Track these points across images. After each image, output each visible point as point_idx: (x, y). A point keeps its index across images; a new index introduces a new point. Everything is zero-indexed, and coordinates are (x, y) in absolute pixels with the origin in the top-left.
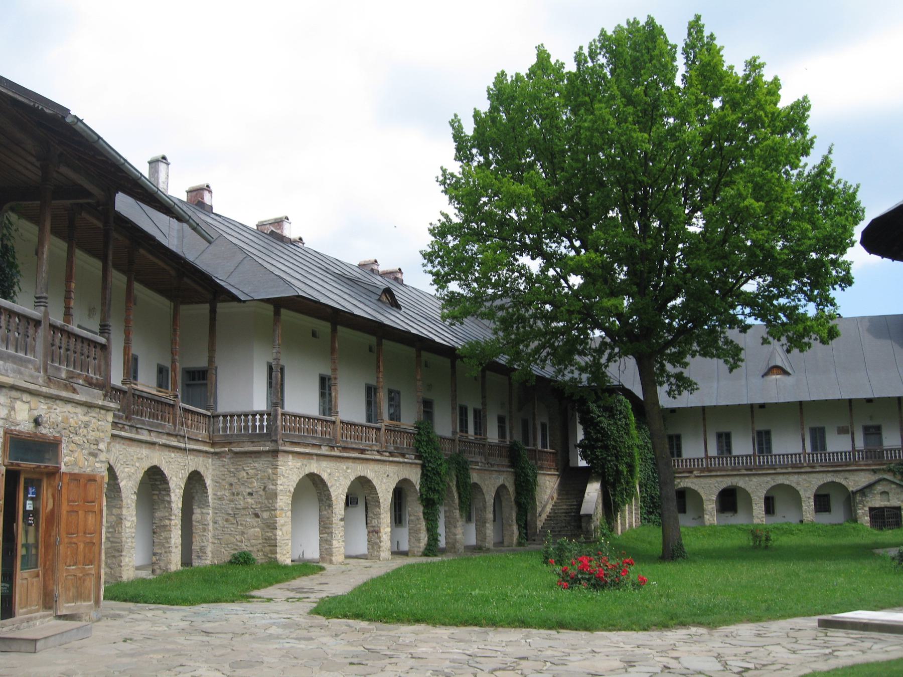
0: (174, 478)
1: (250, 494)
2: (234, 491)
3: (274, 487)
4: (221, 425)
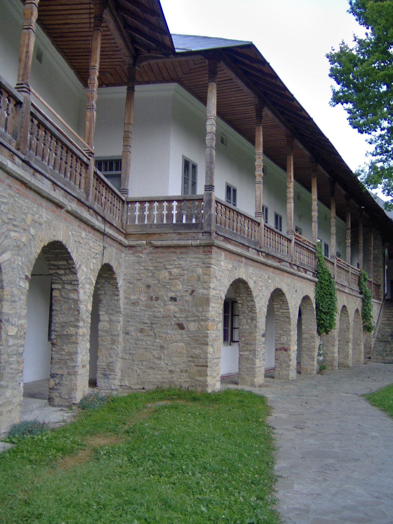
0: (84, 268)
1: (174, 299)
2: (152, 294)
3: (205, 292)
4: (137, 213)
